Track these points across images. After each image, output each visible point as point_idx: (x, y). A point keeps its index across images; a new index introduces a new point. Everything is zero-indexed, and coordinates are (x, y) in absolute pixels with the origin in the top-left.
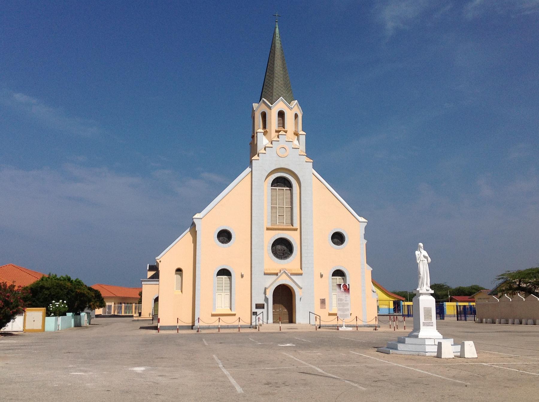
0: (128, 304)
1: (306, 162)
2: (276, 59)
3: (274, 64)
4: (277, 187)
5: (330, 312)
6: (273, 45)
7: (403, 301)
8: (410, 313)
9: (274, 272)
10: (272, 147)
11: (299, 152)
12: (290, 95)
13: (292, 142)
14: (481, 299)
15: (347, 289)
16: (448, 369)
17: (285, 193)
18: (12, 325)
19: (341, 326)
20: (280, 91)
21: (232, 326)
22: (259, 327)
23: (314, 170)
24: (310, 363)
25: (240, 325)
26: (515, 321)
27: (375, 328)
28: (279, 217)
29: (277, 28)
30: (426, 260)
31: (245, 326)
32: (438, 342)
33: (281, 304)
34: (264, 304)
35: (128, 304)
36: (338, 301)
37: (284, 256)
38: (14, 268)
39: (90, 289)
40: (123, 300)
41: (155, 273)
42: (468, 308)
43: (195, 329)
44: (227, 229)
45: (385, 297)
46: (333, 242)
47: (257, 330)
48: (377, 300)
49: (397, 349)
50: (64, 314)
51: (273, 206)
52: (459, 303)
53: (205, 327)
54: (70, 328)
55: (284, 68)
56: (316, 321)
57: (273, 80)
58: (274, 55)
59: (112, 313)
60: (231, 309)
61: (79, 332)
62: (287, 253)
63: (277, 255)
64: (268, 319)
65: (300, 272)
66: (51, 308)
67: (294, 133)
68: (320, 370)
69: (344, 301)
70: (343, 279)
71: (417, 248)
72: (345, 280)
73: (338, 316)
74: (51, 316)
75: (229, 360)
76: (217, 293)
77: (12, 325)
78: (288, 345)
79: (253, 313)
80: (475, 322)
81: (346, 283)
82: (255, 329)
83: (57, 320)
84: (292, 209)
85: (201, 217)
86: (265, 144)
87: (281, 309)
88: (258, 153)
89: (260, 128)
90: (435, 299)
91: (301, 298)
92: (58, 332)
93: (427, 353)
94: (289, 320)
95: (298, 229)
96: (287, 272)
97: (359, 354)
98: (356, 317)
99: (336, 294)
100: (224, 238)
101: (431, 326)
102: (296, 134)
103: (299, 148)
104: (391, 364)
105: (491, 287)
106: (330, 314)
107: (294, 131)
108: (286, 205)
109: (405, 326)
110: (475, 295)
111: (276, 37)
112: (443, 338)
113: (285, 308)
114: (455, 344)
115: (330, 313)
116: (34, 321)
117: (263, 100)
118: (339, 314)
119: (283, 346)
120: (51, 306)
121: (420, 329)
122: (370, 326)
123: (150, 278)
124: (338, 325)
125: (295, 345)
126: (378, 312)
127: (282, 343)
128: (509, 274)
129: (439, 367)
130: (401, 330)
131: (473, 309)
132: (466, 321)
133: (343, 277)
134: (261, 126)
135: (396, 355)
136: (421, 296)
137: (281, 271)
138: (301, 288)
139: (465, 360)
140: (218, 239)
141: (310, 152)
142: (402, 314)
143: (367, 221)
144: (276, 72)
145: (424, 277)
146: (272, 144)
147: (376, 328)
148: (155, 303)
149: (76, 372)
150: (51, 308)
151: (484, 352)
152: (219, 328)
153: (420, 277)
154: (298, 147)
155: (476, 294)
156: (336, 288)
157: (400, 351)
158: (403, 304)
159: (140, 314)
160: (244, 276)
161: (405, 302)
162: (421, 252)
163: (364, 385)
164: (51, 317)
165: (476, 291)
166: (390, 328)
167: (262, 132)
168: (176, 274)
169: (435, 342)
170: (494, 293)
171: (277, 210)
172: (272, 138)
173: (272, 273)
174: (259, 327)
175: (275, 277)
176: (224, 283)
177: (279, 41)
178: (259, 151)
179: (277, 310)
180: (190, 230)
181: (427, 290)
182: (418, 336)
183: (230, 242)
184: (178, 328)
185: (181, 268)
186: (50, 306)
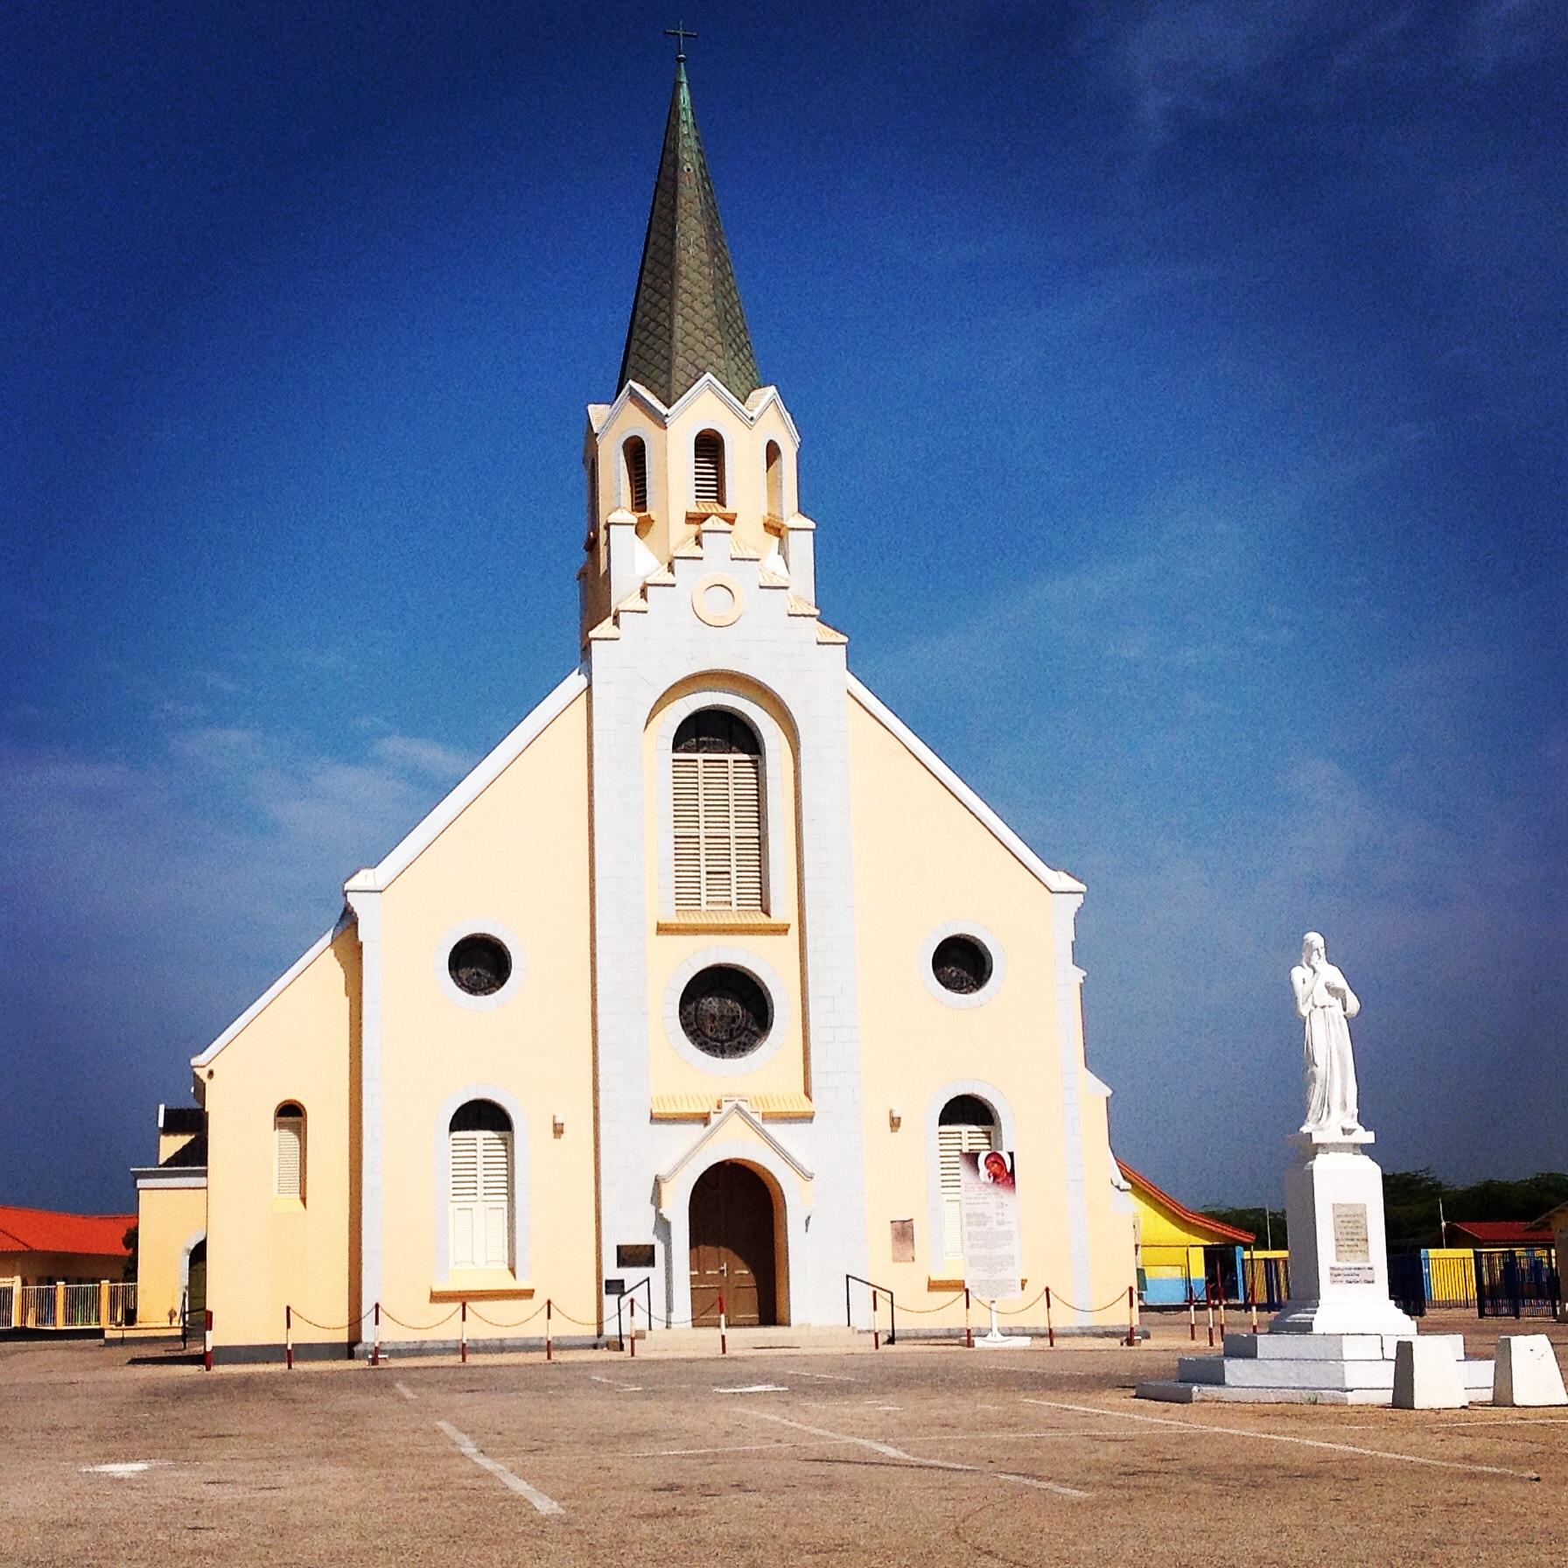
1: (819, 643)
3: (672, 238)
4: (697, 751)
5: (437, 1288)
6: (669, 158)
7: (1246, 1247)
10: (673, 585)
12: (751, 374)
13: (757, 560)
15: (1004, 1175)
29: (685, 85)
30: (1338, 1003)
31: (578, 1343)
33: (726, 1246)
41: (192, 1140)
42: (1523, 1270)
43: (364, 1356)
44: (487, 932)
46: (939, 979)
48: (1137, 1246)
49: (1224, 1383)
55: (716, 254)
57: (671, 304)
58: (675, 198)
59: (15, 1322)
60: (512, 1270)
62: (746, 1029)
64: (669, 1309)
65: (804, 1106)
67: (765, 524)
70: (988, 1135)
71: (1296, 952)
79: (606, 1286)
81: (1001, 1149)
84: (762, 842)
86: (643, 574)
87: (725, 1268)
93: (1348, 1393)
94: (760, 1314)
95: (789, 925)
100: (479, 970)
101: (1369, 1282)
103: (786, 588)
106: (934, 1286)
107: (766, 515)
108: (738, 829)
110: (1552, 1217)
117: (631, 388)
123: (168, 1163)
133: (986, 1128)
136: (1318, 1156)
139: (1516, 1413)
140: (452, 977)
143: (1083, 888)
144: (683, 268)
148: (195, 1267)
159: (131, 1317)
160: (565, 1130)
163: (1082, 1485)
166: (969, 1331)
167: (632, 524)
168: (279, 1125)
169: (1382, 1349)
172: (673, 544)
175: (698, 1130)
177: (692, 142)
178: (619, 602)
179: (708, 1272)
182: (1311, 1324)
183: (505, 986)
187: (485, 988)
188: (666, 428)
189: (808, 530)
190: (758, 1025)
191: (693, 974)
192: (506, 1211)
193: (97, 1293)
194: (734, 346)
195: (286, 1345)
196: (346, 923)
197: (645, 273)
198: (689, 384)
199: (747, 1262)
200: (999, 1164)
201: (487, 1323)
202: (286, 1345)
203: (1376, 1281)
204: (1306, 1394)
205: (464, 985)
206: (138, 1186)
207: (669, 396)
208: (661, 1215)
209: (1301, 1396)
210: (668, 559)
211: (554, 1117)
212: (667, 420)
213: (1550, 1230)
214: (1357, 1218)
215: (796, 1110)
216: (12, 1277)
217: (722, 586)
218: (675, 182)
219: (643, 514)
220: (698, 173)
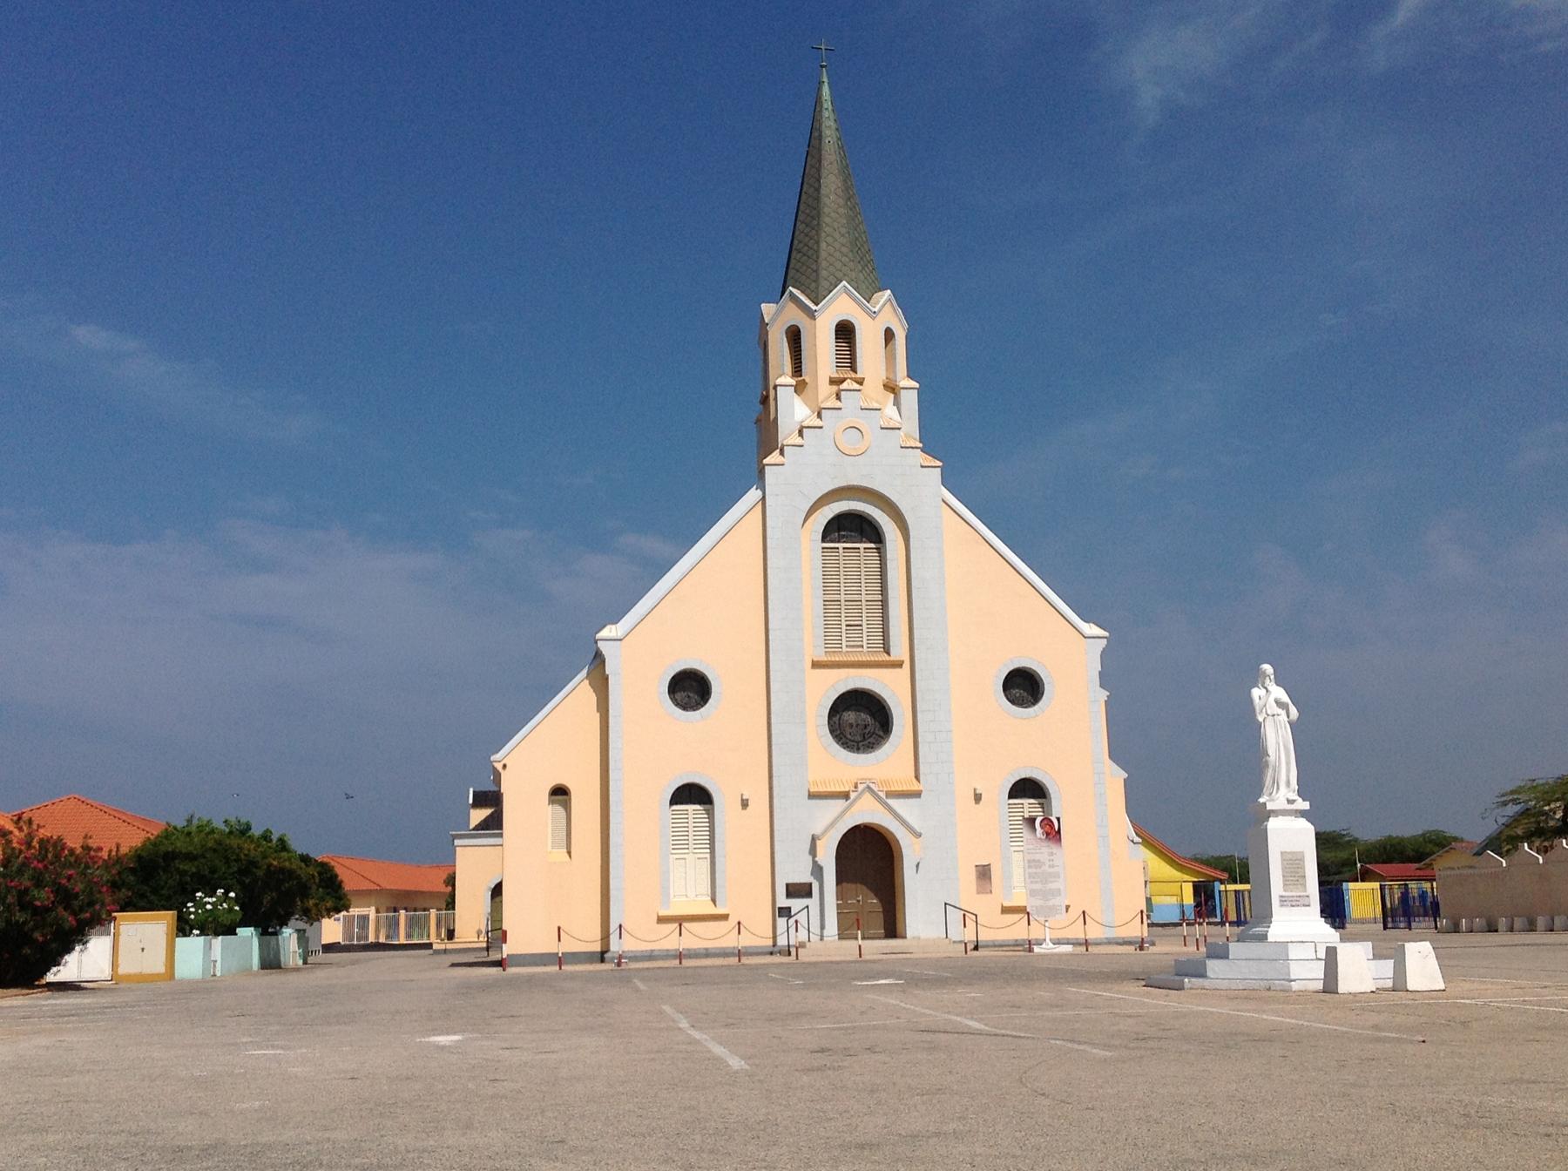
1: (922, 467)
2: (824, 172)
3: (818, 190)
4: (839, 542)
5: (1007, 904)
6: (816, 134)
7: (1222, 882)
8: (1242, 916)
9: (838, 789)
10: (821, 427)
13: (879, 409)
15: (1053, 833)
17: (862, 558)
18: (80, 962)
19: (1039, 943)
21: (718, 951)
23: (945, 490)
28: (848, 628)
29: (826, 84)
30: (1283, 713)
33: (861, 883)
34: (811, 884)
35: (415, 910)
37: (866, 742)
38: (84, 806)
39: (305, 859)
40: (401, 900)
41: (492, 813)
43: (612, 960)
44: (695, 667)
45: (1167, 871)
46: (1008, 699)
48: (1146, 882)
50: (230, 931)
51: (828, 597)
54: (247, 971)
59: (371, 939)
63: (844, 739)
64: (822, 927)
65: (915, 787)
66: (191, 913)
67: (884, 386)
69: (1046, 868)
70: (1042, 805)
71: (1256, 678)
76: (672, 854)
77: (80, 962)
81: (1052, 816)
82: (785, 956)
83: (208, 948)
84: (884, 603)
85: (620, 635)
86: (800, 420)
87: (860, 898)
88: (779, 446)
89: (783, 374)
92: (214, 981)
93: (1293, 983)
95: (903, 662)
96: (876, 789)
99: (1022, 849)
101: (1304, 905)
102: (891, 388)
103: (899, 429)
105: (1478, 829)
106: (1006, 910)
108: (869, 593)
113: (872, 895)
114: (1377, 956)
115: (1004, 905)
116: (143, 949)
118: (1032, 907)
119: (867, 985)
120: (192, 907)
121: (1272, 917)
122: (1129, 943)
123: (476, 828)
131: (1429, 900)
132: (1410, 929)
133: (1041, 801)
134: (788, 366)
136: (1271, 819)
137: (859, 785)
138: (918, 835)
139: (1410, 996)
140: (671, 698)
141: (931, 441)
143: (1106, 634)
144: (826, 210)
145: (1280, 764)
153: (1267, 762)
154: (898, 425)
159: (451, 935)
162: (1267, 691)
165: (1435, 849)
167: (792, 386)
168: (551, 802)
169: (1316, 952)
171: (839, 583)
172: (820, 401)
173: (836, 792)
175: (840, 804)
177: (832, 123)
179: (849, 902)
180: (588, 674)
182: (1266, 935)
183: (708, 704)
186: (189, 907)
188: (815, 319)
192: (709, 860)
195: (558, 954)
196: (596, 663)
199: (876, 895)
201: (697, 937)
202: (558, 954)
203: (1312, 904)
206: (456, 844)
207: (817, 297)
208: (816, 862)
212: (816, 314)
213: (1433, 869)
215: (909, 788)
216: (369, 907)
218: (820, 150)
219: (800, 379)
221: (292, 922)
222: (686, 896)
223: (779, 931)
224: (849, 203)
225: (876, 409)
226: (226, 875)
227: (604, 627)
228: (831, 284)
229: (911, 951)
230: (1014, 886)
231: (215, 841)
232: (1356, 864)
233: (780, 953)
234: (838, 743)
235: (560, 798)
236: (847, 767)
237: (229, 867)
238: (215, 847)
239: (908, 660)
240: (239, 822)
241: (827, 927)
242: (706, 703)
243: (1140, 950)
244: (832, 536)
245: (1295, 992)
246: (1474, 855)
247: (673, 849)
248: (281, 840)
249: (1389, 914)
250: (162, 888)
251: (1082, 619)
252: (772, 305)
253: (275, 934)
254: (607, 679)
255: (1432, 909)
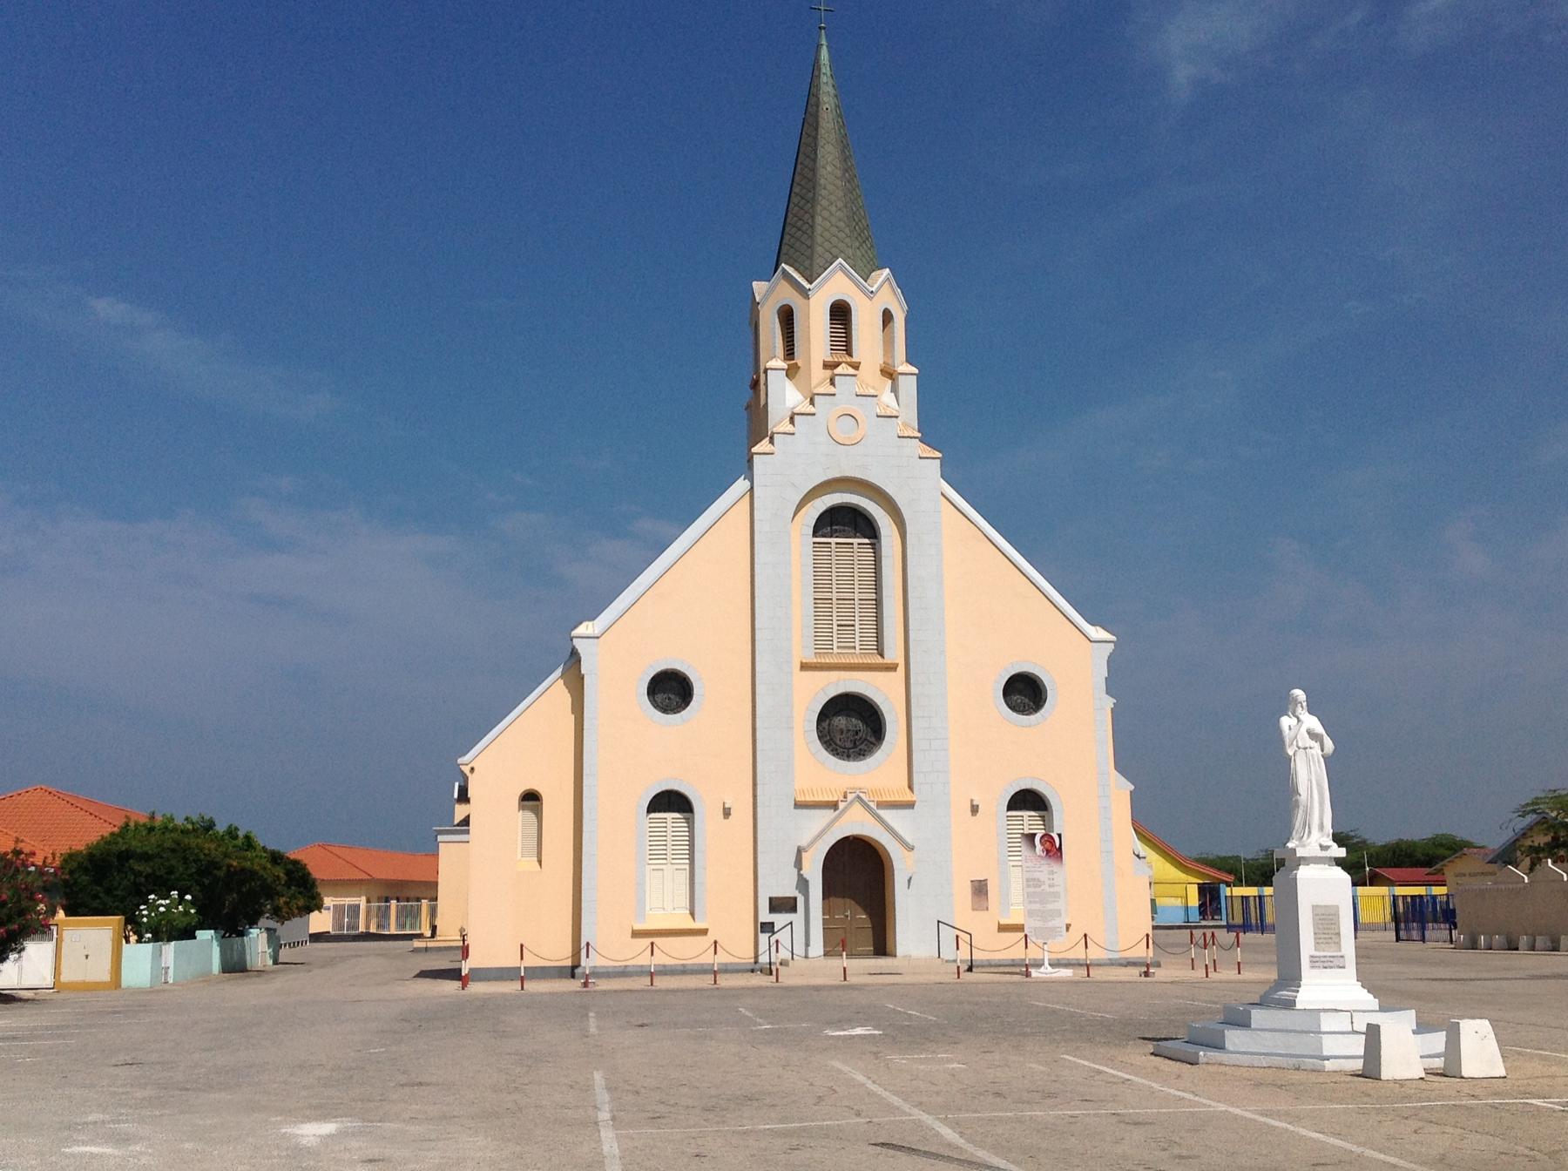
0: (408, 901)
1: (920, 458)
2: (821, 142)
3: (815, 160)
4: (831, 537)
5: (1004, 921)
6: (813, 100)
7: (1228, 884)
9: (826, 799)
10: (814, 414)
11: (897, 427)
13: (876, 396)
14: (1464, 875)
15: (1054, 850)
16: (1413, 1124)
17: (856, 554)
19: (1038, 964)
20: (834, 240)
22: (777, 970)
23: (946, 483)
24: (920, 1105)
25: (718, 964)
26: (1537, 941)
27: (1146, 969)
28: (839, 628)
29: (825, 48)
30: (1317, 745)
32: (1368, 1024)
34: (795, 899)
36: (1028, 886)
39: (276, 858)
45: (1173, 873)
46: (1008, 705)
47: (773, 978)
48: (1150, 884)
50: (188, 934)
52: (1395, 888)
53: (610, 970)
54: (206, 978)
55: (847, 171)
56: (958, 948)
59: (362, 929)
61: (241, 991)
64: (807, 944)
65: (908, 797)
66: (143, 916)
67: (881, 371)
68: (948, 1133)
69: (1046, 887)
70: (1043, 817)
71: (1285, 705)
72: (1047, 821)
73: (1026, 932)
74: (145, 942)
75: (643, 1091)
78: (859, 1031)
79: (761, 927)
80: (1453, 946)
81: (1053, 832)
82: (766, 974)
83: (157, 956)
84: (878, 603)
85: (597, 633)
86: (792, 406)
89: (775, 357)
90: (1349, 877)
91: (911, 878)
93: (1326, 1062)
95: (897, 665)
97: (1092, 1065)
98: (1085, 935)
99: (1020, 863)
101: (1341, 967)
103: (897, 417)
104: (1205, 1105)
105: (1496, 840)
106: (1003, 928)
109: (1239, 963)
110: (1445, 865)
111: (822, 75)
112: (1382, 1009)
114: (1422, 1028)
115: (1001, 923)
116: (87, 957)
117: (783, 268)
124: (1027, 962)
125: (881, 1032)
126: (1153, 919)
127: (840, 1023)
128: (1555, 797)
129: (1380, 1118)
130: (1227, 974)
132: (1424, 942)
133: (1042, 813)
135: (1222, 1069)
136: (1301, 867)
138: (912, 849)
140: (650, 701)
141: (931, 429)
142: (1225, 923)
144: (822, 181)
146: (814, 406)
147: (1148, 969)
149: (92, 1142)
150: (143, 916)
151: (1519, 1053)
152: (652, 975)
153: (1297, 801)
154: (895, 413)
155: (1450, 862)
156: (1020, 851)
157: (1232, 1053)
158: (1229, 894)
161: (1234, 888)
162: (1299, 720)
164: (144, 944)
165: (1447, 853)
166: (1193, 969)
167: (783, 369)
168: (522, 808)
169: (1352, 1023)
170: (1506, 856)
174: (777, 970)
175: (829, 814)
176: (669, 838)
177: (830, 89)
178: (774, 427)
180: (562, 674)
181: (1321, 846)
182: (1295, 1001)
183: (689, 708)
184: (523, 974)
185: (537, 789)
187: (674, 709)
189: (912, 374)
190: (875, 737)
191: (827, 700)
193: (419, 908)
194: (859, 238)
196: (573, 660)
197: (795, 184)
198: (826, 266)
199: (865, 910)
200: (1050, 842)
201: (674, 952)
203: (1347, 966)
204: (1292, 1061)
205: (658, 706)
206: (439, 840)
207: (811, 276)
208: (802, 875)
209: (1288, 1064)
210: (810, 395)
211: (724, 803)
212: (810, 293)
213: (1443, 874)
214: (1331, 917)
215: (901, 799)
216: (360, 897)
217: (850, 415)
218: (816, 117)
219: (792, 362)
220: (834, 111)
221: (263, 922)
222: (664, 909)
223: (761, 950)
224: (847, 175)
225: (873, 396)
226: (184, 876)
227: (581, 623)
228: (827, 261)
229: (899, 972)
230: (1012, 904)
231: (174, 841)
232: (1365, 867)
233: (761, 971)
234: (826, 749)
235: (531, 803)
236: (835, 775)
237: (186, 869)
238: (173, 846)
239: (903, 662)
240: (203, 818)
241: (811, 943)
242: (687, 704)
243: (1145, 976)
244: (824, 530)
245: (1328, 1072)
246: (1489, 862)
247: (650, 859)
248: (247, 837)
249: (1402, 919)
250: (116, 889)
251: (1089, 623)
252: (763, 283)
253: (242, 934)
254: (583, 678)
255: (1449, 917)
